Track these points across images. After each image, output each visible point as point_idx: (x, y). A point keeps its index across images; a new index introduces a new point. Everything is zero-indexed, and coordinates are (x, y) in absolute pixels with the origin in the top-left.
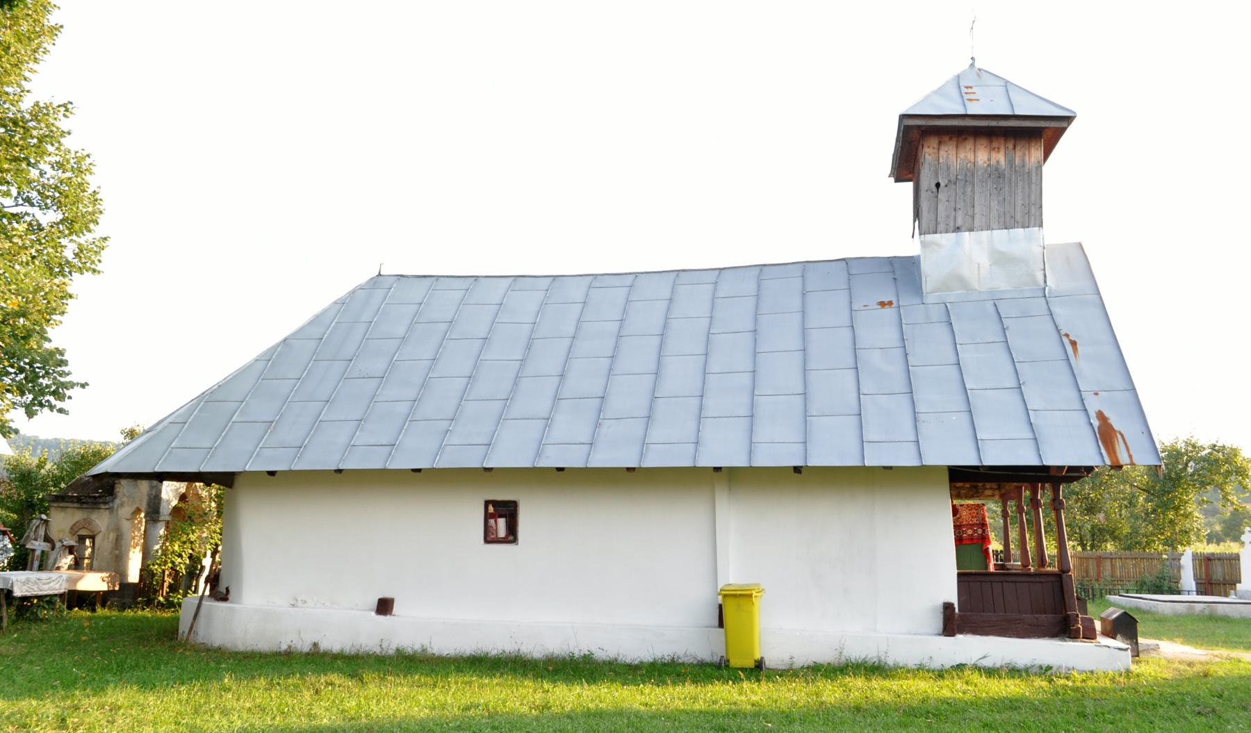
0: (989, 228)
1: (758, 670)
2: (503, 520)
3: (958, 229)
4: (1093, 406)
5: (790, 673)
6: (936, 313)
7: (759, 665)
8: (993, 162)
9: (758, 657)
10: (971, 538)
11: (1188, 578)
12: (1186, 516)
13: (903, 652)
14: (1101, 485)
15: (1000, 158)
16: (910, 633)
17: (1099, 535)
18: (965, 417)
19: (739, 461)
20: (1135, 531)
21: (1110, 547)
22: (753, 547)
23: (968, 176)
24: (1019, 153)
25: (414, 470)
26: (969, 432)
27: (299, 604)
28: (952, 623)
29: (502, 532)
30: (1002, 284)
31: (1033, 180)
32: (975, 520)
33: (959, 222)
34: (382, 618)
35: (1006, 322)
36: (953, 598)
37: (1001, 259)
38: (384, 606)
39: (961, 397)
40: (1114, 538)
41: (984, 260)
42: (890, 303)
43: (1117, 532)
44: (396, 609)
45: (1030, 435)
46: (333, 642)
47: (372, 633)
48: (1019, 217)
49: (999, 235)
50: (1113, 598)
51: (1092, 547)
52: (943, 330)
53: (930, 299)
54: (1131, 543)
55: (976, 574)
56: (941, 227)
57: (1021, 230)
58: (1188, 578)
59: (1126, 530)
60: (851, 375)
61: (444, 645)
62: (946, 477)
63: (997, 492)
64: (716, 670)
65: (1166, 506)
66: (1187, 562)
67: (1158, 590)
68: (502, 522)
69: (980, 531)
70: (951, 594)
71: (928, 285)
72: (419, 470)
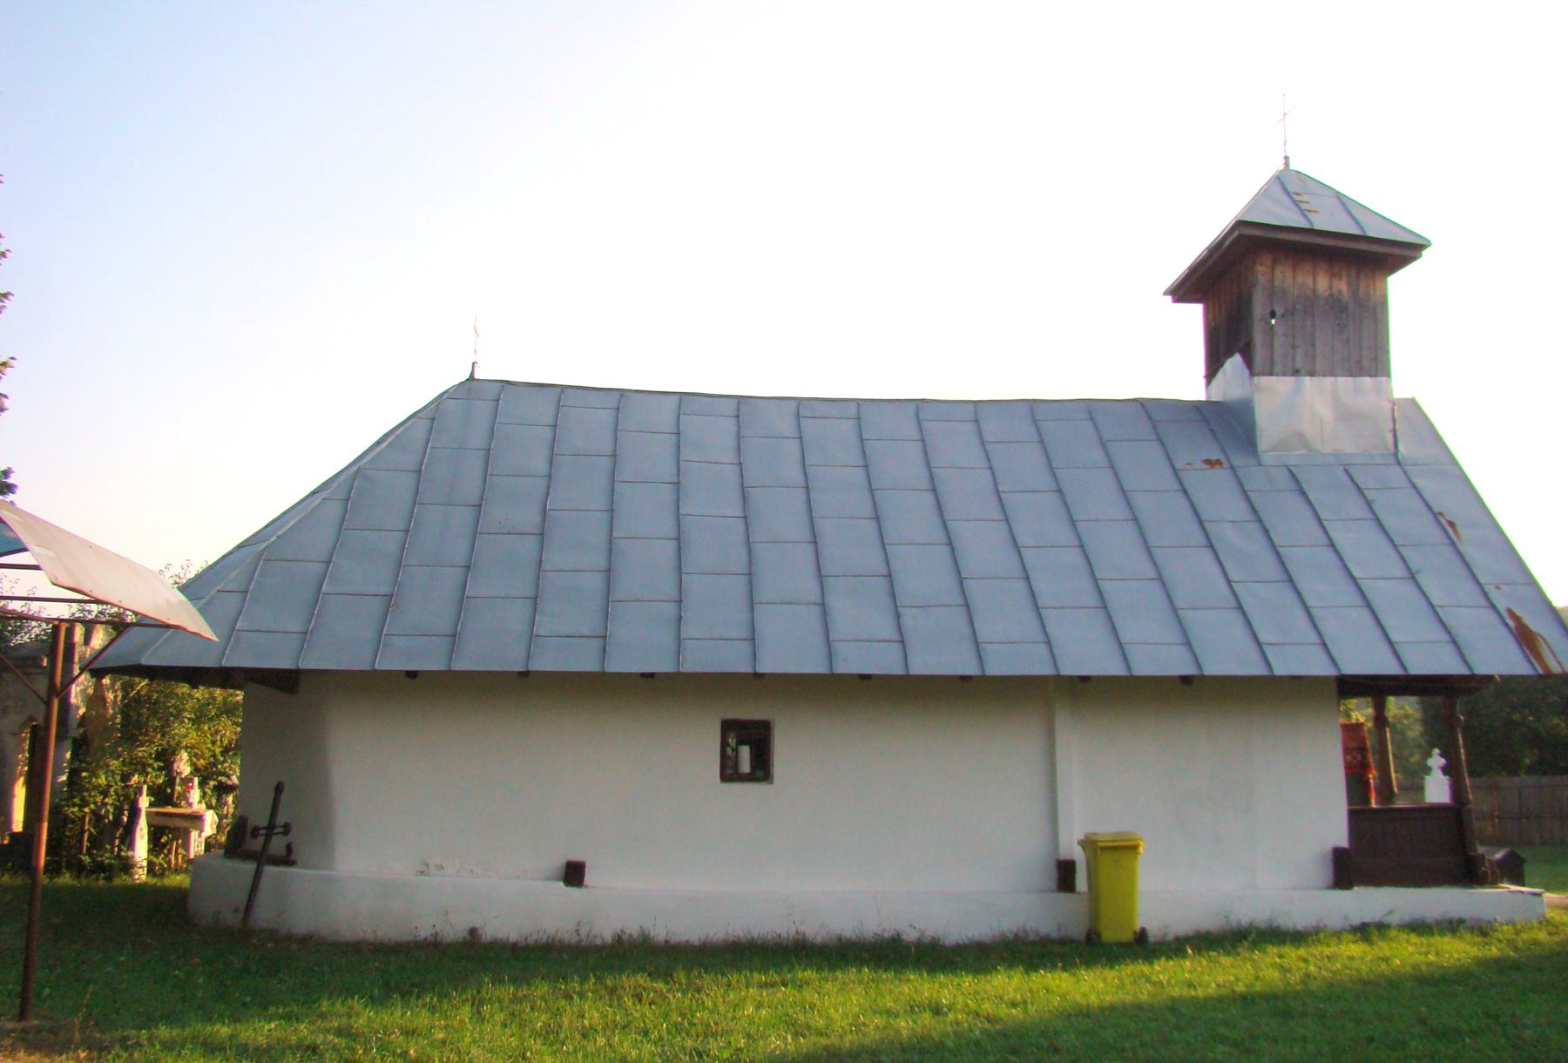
0: (1332, 374)
1: (1142, 946)
2: (749, 752)
3: (1296, 373)
4: (1501, 606)
5: (1175, 947)
6: (1282, 478)
7: (1141, 936)
8: (1334, 290)
9: (1137, 928)
13: (1298, 916)
15: (1342, 286)
16: (1294, 888)
18: (1365, 612)
19: (664, 665)
22: (1105, 784)
23: (1310, 304)
24: (1362, 283)
25: (643, 675)
26: (1377, 633)
27: (432, 870)
28: (1347, 869)
29: (745, 767)
30: (1348, 446)
31: (1373, 316)
33: (1299, 365)
34: (573, 891)
35: (1370, 495)
36: (1343, 841)
37: (1346, 415)
38: (574, 874)
39: (1351, 589)
41: (1325, 411)
42: (1218, 462)
44: (588, 879)
46: (502, 925)
47: (552, 912)
48: (1365, 363)
49: (1344, 382)
52: (1295, 501)
53: (1267, 459)
56: (1278, 368)
57: (1367, 380)
60: (1206, 557)
61: (690, 928)
62: (1334, 689)
64: (1090, 947)
68: (745, 752)
70: (1341, 838)
71: (1264, 442)
72: (652, 675)
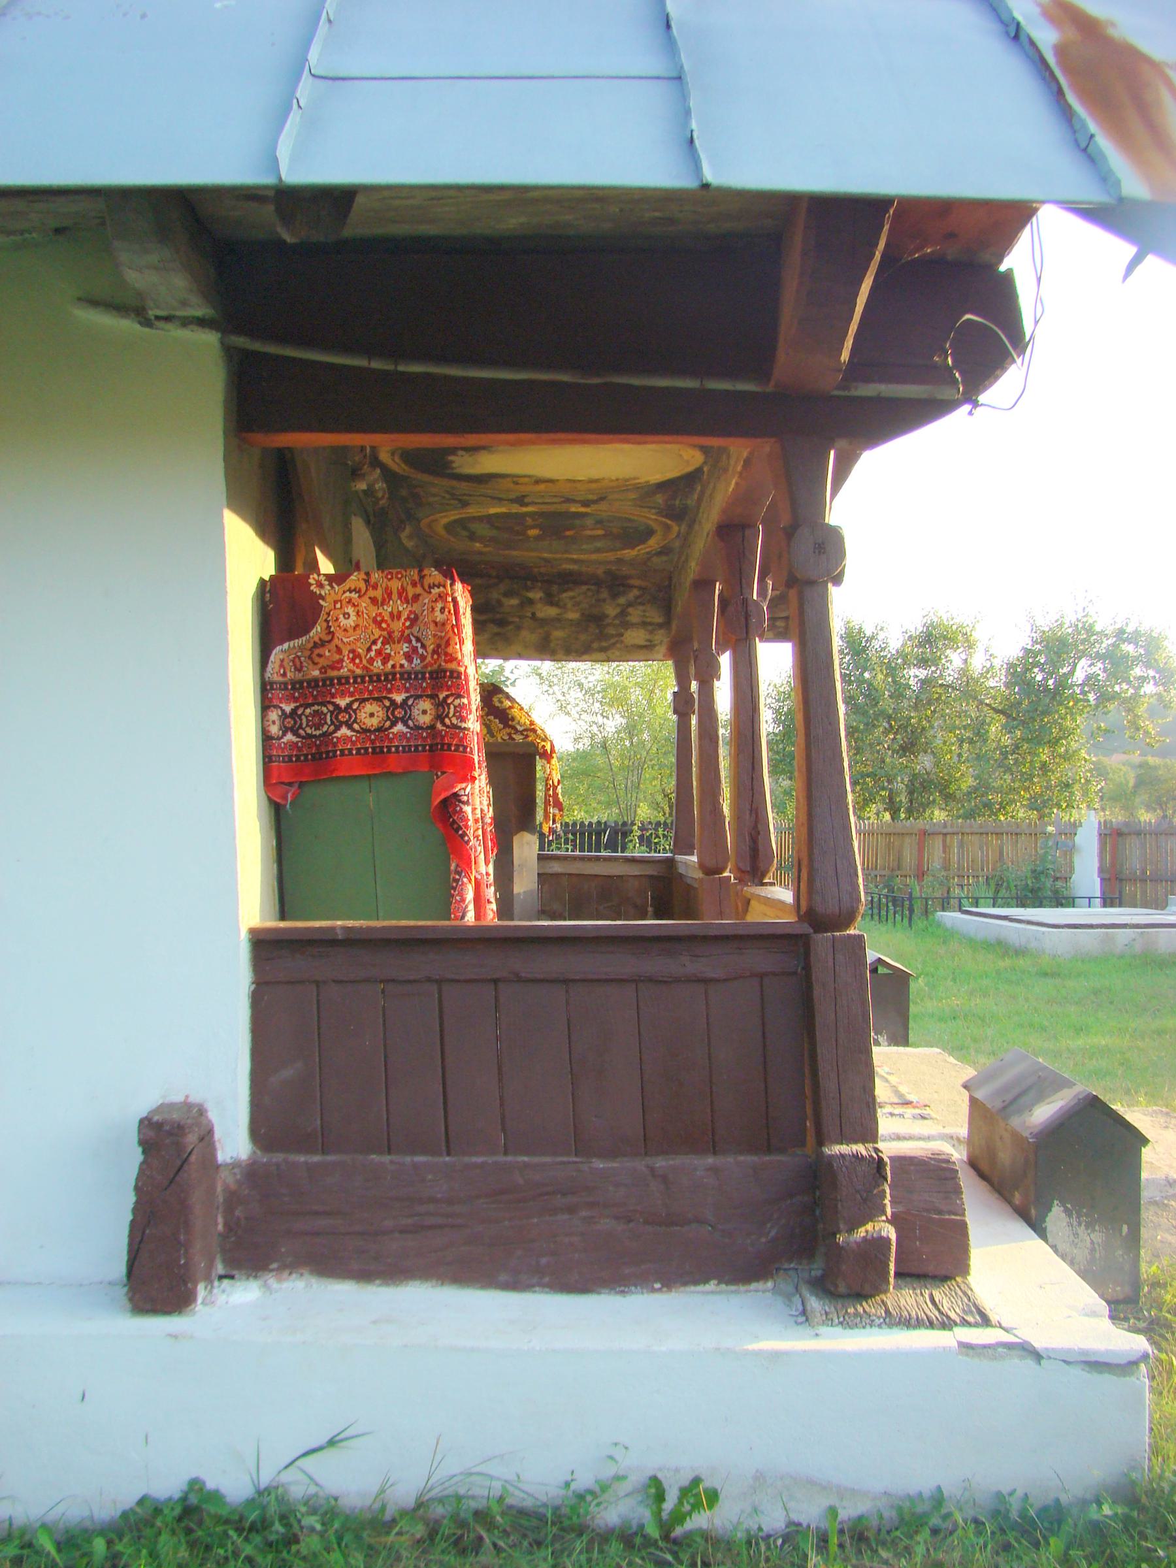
10: (376, 752)
11: (1086, 874)
12: (1067, 757)
14: (929, 703)
17: (922, 790)
20: (982, 787)
21: (939, 815)
28: (179, 1228)
32: (398, 654)
40: (948, 797)
43: (953, 787)
45: (653, 63)
50: (951, 917)
51: (909, 811)
54: (980, 803)
55: (354, 942)
58: (1086, 874)
59: (968, 783)
63: (661, 637)
65: (1037, 739)
66: (1088, 843)
67: (1032, 896)
69: (423, 714)
70: (211, 1067)
